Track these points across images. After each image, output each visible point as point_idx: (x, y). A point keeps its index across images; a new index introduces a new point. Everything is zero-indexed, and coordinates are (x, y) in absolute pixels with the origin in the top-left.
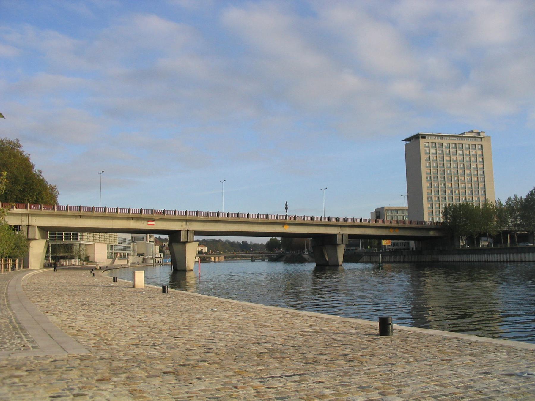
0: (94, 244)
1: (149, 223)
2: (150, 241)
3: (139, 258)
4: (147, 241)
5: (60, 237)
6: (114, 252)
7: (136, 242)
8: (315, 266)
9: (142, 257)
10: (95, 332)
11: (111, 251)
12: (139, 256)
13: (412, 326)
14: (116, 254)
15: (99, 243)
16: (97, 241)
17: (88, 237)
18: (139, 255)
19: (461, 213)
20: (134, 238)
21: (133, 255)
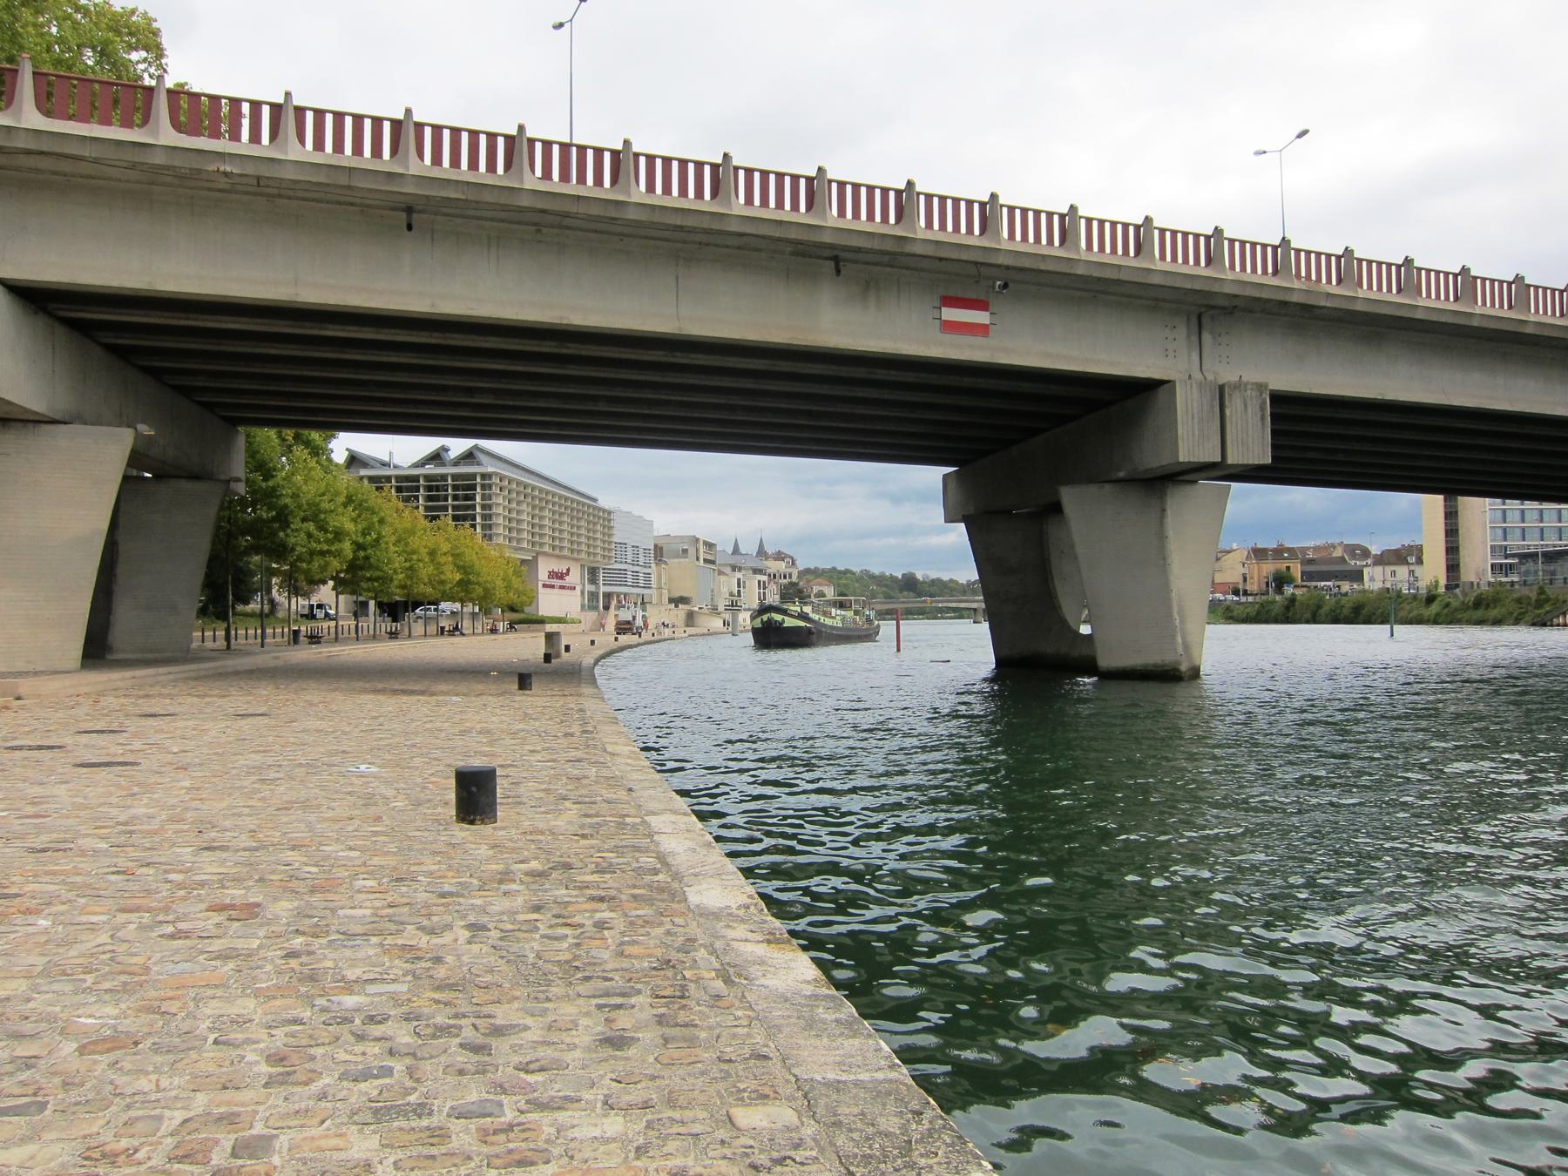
0: (535, 559)
1: (950, 314)
2: (706, 561)
3: (675, 611)
4: (698, 559)
5: (436, 498)
6: (603, 589)
7: (665, 563)
8: (985, 661)
9: (686, 607)
10: (657, 721)
11: (592, 588)
12: (676, 606)
13: (1044, 1066)
14: (608, 596)
15: (553, 556)
16: (546, 549)
17: (514, 534)
18: (677, 601)
19: (1130, 878)
20: (661, 549)
21: (660, 603)
